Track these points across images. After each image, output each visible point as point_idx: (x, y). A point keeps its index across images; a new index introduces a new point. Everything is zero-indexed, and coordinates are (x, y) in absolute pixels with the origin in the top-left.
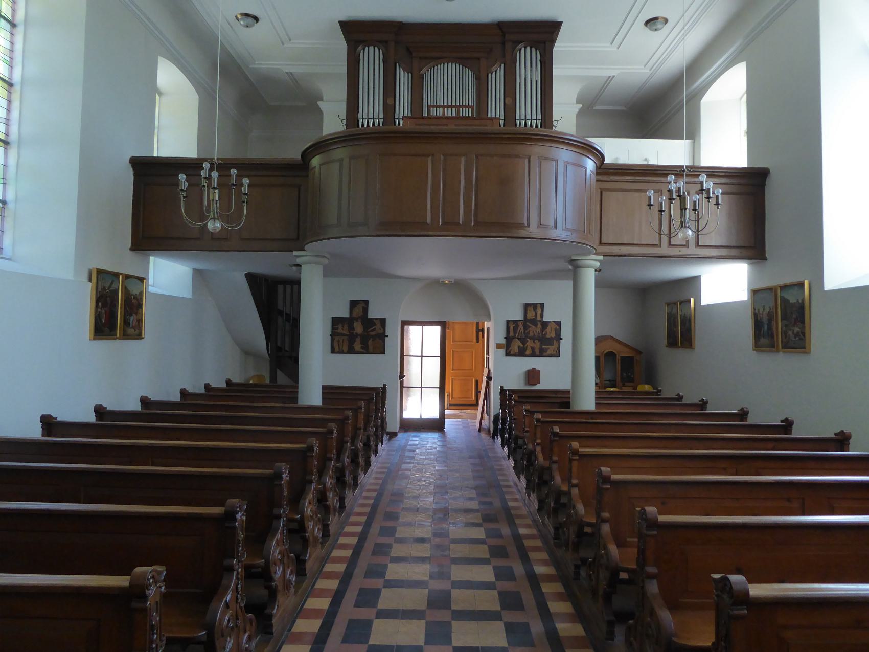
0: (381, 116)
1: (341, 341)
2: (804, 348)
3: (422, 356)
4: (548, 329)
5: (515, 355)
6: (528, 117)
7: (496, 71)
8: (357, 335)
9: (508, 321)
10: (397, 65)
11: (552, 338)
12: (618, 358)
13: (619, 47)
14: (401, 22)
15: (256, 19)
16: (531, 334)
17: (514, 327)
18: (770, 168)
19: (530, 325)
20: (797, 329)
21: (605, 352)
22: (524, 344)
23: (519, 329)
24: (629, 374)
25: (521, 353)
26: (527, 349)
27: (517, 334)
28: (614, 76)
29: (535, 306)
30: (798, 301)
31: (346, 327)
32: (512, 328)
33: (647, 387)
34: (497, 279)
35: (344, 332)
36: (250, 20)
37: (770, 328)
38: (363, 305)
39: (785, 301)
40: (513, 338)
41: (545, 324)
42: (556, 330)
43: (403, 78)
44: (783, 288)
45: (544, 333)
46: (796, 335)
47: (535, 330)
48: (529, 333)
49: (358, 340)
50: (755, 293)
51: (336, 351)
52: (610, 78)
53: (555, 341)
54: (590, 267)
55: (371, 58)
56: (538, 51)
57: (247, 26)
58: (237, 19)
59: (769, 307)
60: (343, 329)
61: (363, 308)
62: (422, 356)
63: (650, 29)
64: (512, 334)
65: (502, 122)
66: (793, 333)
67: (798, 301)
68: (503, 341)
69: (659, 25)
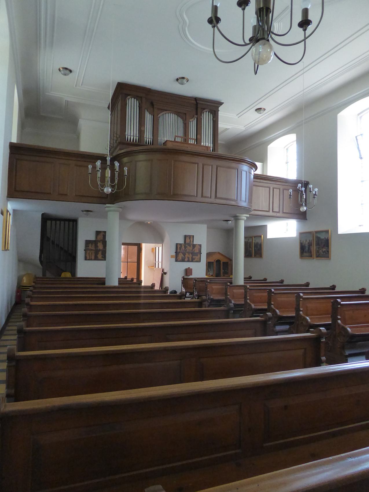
0: (138, 135)
1: (90, 253)
2: (328, 257)
3: (127, 262)
4: (196, 248)
5: (180, 261)
6: (132, 134)
7: (193, 121)
8: (100, 250)
9: (177, 244)
10: (146, 110)
11: (197, 253)
12: (222, 263)
13: (239, 117)
14: (150, 89)
15: (71, 71)
16: (188, 251)
17: (180, 247)
18: (309, 181)
19: (187, 246)
20: (324, 250)
21: (216, 260)
22: (184, 256)
23: (182, 248)
24: (226, 270)
25: (183, 260)
26: (185, 258)
27: (181, 251)
28: (229, 129)
29: (190, 237)
30: (325, 238)
31: (93, 245)
32: (179, 247)
33: (68, 275)
34: (174, 222)
35: (92, 248)
36: (68, 72)
37: (309, 249)
38: (103, 234)
39: (318, 238)
40: (180, 252)
41: (194, 246)
42: (199, 249)
43: (148, 117)
44: (316, 232)
45: (193, 250)
46: (324, 252)
47: (189, 249)
48: (187, 250)
49: (100, 253)
50: (301, 234)
51: (87, 259)
52: (227, 129)
53: (198, 254)
54: (242, 220)
55: (132, 105)
56: (137, 101)
57: (65, 75)
58: (59, 70)
59: (309, 240)
60: (92, 247)
61: (103, 235)
62: (127, 262)
63: (258, 113)
64: (178, 251)
65: (211, 149)
66: (322, 251)
67: (325, 238)
68: (174, 254)
69: (185, 81)
